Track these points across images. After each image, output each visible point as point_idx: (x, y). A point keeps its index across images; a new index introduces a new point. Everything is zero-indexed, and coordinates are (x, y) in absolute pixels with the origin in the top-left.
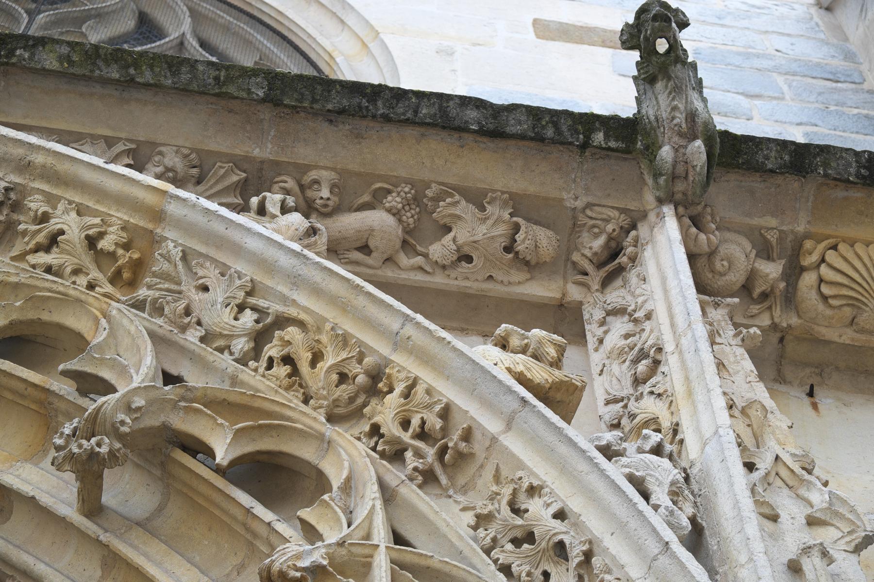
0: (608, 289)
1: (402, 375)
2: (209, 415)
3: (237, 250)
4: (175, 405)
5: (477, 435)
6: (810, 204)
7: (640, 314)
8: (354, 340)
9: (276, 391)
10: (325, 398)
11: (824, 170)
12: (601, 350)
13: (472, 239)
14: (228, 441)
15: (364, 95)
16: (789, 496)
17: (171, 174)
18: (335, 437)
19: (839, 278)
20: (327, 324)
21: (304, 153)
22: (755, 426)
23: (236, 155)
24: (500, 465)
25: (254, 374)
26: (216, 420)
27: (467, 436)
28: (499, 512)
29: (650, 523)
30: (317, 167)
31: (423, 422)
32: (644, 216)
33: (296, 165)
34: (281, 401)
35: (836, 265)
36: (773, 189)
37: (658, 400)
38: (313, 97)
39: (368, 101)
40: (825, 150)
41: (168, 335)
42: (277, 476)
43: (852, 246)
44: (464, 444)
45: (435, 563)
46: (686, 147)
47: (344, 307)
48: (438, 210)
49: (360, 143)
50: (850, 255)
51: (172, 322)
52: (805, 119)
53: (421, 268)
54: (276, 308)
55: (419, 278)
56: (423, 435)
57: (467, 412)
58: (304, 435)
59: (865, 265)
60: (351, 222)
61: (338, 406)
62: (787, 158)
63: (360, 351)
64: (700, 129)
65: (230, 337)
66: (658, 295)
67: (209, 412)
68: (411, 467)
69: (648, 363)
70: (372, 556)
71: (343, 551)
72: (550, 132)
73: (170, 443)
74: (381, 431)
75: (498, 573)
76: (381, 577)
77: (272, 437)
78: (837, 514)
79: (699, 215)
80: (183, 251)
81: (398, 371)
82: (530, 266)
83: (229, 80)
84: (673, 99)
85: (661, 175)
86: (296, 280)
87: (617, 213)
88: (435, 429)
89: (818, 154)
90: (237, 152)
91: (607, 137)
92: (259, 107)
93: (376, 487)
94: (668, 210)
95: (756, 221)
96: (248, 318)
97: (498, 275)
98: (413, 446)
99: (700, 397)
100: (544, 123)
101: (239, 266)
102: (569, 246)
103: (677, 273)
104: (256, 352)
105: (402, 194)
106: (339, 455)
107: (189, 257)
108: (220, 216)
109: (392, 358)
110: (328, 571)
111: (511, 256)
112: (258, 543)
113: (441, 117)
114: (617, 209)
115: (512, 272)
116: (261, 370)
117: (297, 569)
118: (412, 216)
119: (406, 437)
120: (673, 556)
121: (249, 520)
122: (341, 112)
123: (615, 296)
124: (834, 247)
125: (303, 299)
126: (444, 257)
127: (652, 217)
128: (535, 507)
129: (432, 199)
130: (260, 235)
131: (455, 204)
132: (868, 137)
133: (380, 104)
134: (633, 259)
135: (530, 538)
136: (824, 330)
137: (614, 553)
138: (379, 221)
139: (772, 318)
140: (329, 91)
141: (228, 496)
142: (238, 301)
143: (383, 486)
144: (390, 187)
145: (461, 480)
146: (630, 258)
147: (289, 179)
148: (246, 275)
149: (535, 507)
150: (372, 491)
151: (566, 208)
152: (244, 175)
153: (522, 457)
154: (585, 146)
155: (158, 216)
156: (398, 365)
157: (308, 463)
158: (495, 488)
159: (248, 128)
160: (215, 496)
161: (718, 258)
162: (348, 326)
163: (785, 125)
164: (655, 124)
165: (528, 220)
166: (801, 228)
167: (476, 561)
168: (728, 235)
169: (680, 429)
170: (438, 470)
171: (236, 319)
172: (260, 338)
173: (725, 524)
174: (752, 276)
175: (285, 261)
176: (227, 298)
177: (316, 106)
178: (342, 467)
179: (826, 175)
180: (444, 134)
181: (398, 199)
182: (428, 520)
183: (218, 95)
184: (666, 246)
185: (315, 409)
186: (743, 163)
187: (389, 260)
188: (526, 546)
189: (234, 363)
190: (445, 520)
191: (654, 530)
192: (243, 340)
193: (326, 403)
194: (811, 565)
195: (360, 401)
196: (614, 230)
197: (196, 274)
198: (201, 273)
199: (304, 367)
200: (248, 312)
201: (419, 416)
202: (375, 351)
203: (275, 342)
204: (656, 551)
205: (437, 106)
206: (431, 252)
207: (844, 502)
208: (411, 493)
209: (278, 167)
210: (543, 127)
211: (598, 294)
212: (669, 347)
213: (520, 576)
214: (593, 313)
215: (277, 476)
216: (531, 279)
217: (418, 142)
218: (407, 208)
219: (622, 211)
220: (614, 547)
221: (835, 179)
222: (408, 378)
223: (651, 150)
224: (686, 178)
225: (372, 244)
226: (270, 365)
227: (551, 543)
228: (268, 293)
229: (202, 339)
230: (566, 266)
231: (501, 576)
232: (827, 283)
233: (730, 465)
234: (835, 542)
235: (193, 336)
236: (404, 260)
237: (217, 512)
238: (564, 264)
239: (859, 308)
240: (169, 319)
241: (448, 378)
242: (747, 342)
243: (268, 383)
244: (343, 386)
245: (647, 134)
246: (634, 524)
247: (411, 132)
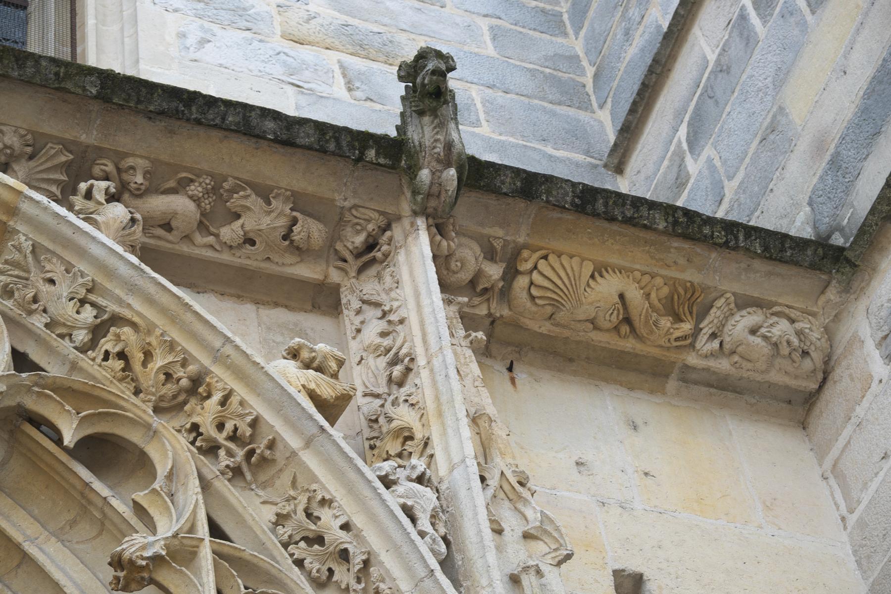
0: (363, 277)
1: (220, 385)
2: (58, 402)
3: (82, 253)
4: (29, 389)
5: (280, 446)
6: (531, 220)
7: (393, 317)
8: (180, 348)
9: (111, 382)
10: (153, 394)
11: (547, 197)
12: (358, 339)
13: (257, 227)
14: (74, 426)
15: (181, 100)
16: (510, 509)
17: (8, 151)
18: (161, 429)
19: (546, 283)
20: (157, 329)
21: (123, 142)
22: (483, 435)
23: (66, 139)
25: (92, 363)
26: (64, 406)
27: (271, 445)
28: (295, 513)
29: (419, 551)
30: (133, 155)
31: (236, 429)
32: (399, 218)
33: (116, 152)
34: (113, 391)
35: (545, 273)
37: (411, 409)
38: (138, 99)
39: (184, 106)
40: (549, 179)
41: (17, 317)
42: (106, 452)
43: (559, 257)
44: (269, 452)
45: (246, 556)
46: (441, 172)
47: (173, 319)
48: (232, 200)
49: (172, 138)
50: (557, 266)
51: (19, 305)
52: (490, 12)
53: (212, 246)
54: (113, 307)
55: (210, 254)
56: (233, 437)
57: (273, 427)
58: (132, 422)
59: (567, 274)
60: (159, 204)
61: (163, 401)
62: (519, 184)
63: (184, 358)
64: (455, 158)
65: (73, 328)
66: (411, 304)
67: (58, 399)
68: (224, 464)
69: (401, 369)
70: (198, 547)
71: (176, 542)
72: (332, 146)
73: (20, 416)
74: (201, 430)
75: (294, 566)
76: (208, 570)
78: (546, 532)
79: (443, 223)
80: (33, 245)
81: (217, 382)
82: (300, 251)
83: (68, 76)
84: (437, 133)
85: (419, 193)
86: (133, 289)
87: (376, 215)
88: (244, 435)
89: (543, 183)
90: (67, 136)
91: (378, 154)
92: (90, 101)
93: (197, 482)
94: (421, 222)
95: (487, 231)
96: (88, 314)
97: (276, 258)
98: (226, 447)
99: (449, 422)
100: (328, 138)
101: (82, 266)
102: (333, 238)
103: (429, 292)
104: (93, 344)
105: (203, 184)
106: (163, 444)
107: (37, 250)
108: (68, 221)
109: (213, 369)
110: (165, 559)
111: (287, 243)
112: (92, 509)
113: (244, 125)
114: (378, 211)
115: (286, 255)
116: (99, 360)
117: (143, 558)
118: (210, 203)
119: (221, 438)
120: (437, 581)
121: (87, 491)
122: (161, 113)
123: (369, 287)
124: (545, 257)
125: (137, 304)
126: (232, 239)
127: (406, 222)
128: (325, 514)
129: (228, 191)
130: (104, 245)
131: (246, 197)
132: (544, 35)
133: (194, 109)
134: (386, 256)
135: (319, 540)
136: (527, 322)
137: (388, 567)
138: (181, 205)
139: (489, 309)
140: (152, 94)
141: (71, 469)
142: (80, 297)
143: (201, 477)
144: (190, 176)
145: (262, 477)
146: (384, 255)
147: (109, 164)
148: (88, 275)
149: (325, 514)
150: (194, 484)
151: (336, 206)
152: (71, 157)
153: (317, 473)
154: (360, 159)
155: (13, 211)
156: (217, 376)
157: (136, 446)
158: (292, 493)
159: (78, 116)
160: (60, 469)
161: (454, 259)
162: (175, 334)
163: (474, 16)
164: (418, 148)
165: (303, 212)
166: (521, 240)
167: (276, 553)
168: (464, 240)
169: (430, 443)
170: (245, 468)
171: (78, 312)
172: (98, 331)
173: (470, 546)
174: (479, 275)
175: (123, 270)
176: (71, 293)
177: (139, 106)
178: (165, 455)
179: (548, 202)
180: (244, 138)
181: (200, 189)
182: (237, 512)
183: (57, 89)
184: (415, 257)
185: (144, 402)
186: (484, 186)
187: (187, 238)
188: (316, 547)
189: (75, 351)
190: (251, 515)
191: (423, 557)
192: (84, 332)
193: (154, 398)
194: (528, 580)
195: (181, 398)
196: (374, 230)
197: (44, 267)
198: (48, 267)
199: (137, 366)
200: (87, 306)
201: (233, 422)
202: (198, 360)
203: (110, 336)
204: (423, 575)
205: (241, 115)
206: (222, 234)
207: (552, 521)
208: (222, 485)
209: (100, 152)
210: (327, 141)
211: (354, 280)
212: (421, 361)
213: (311, 572)
214: (350, 300)
215: (106, 452)
216: (302, 261)
217: (221, 141)
218: (206, 196)
219: (381, 213)
220: (387, 560)
221: (554, 205)
222: (225, 389)
223: (412, 171)
224: (439, 196)
225: (174, 224)
226: (107, 356)
227: (338, 549)
228: (105, 293)
229: (47, 325)
230: (329, 252)
231: (296, 569)
232: (536, 286)
233: (475, 495)
234: (544, 556)
235: (38, 322)
236: (199, 239)
237: (57, 478)
238: (330, 251)
239: (558, 307)
240: (18, 302)
241: (259, 395)
242: (474, 344)
243: (104, 373)
244: (169, 386)
245: (410, 156)
246: (406, 548)
247: (215, 134)
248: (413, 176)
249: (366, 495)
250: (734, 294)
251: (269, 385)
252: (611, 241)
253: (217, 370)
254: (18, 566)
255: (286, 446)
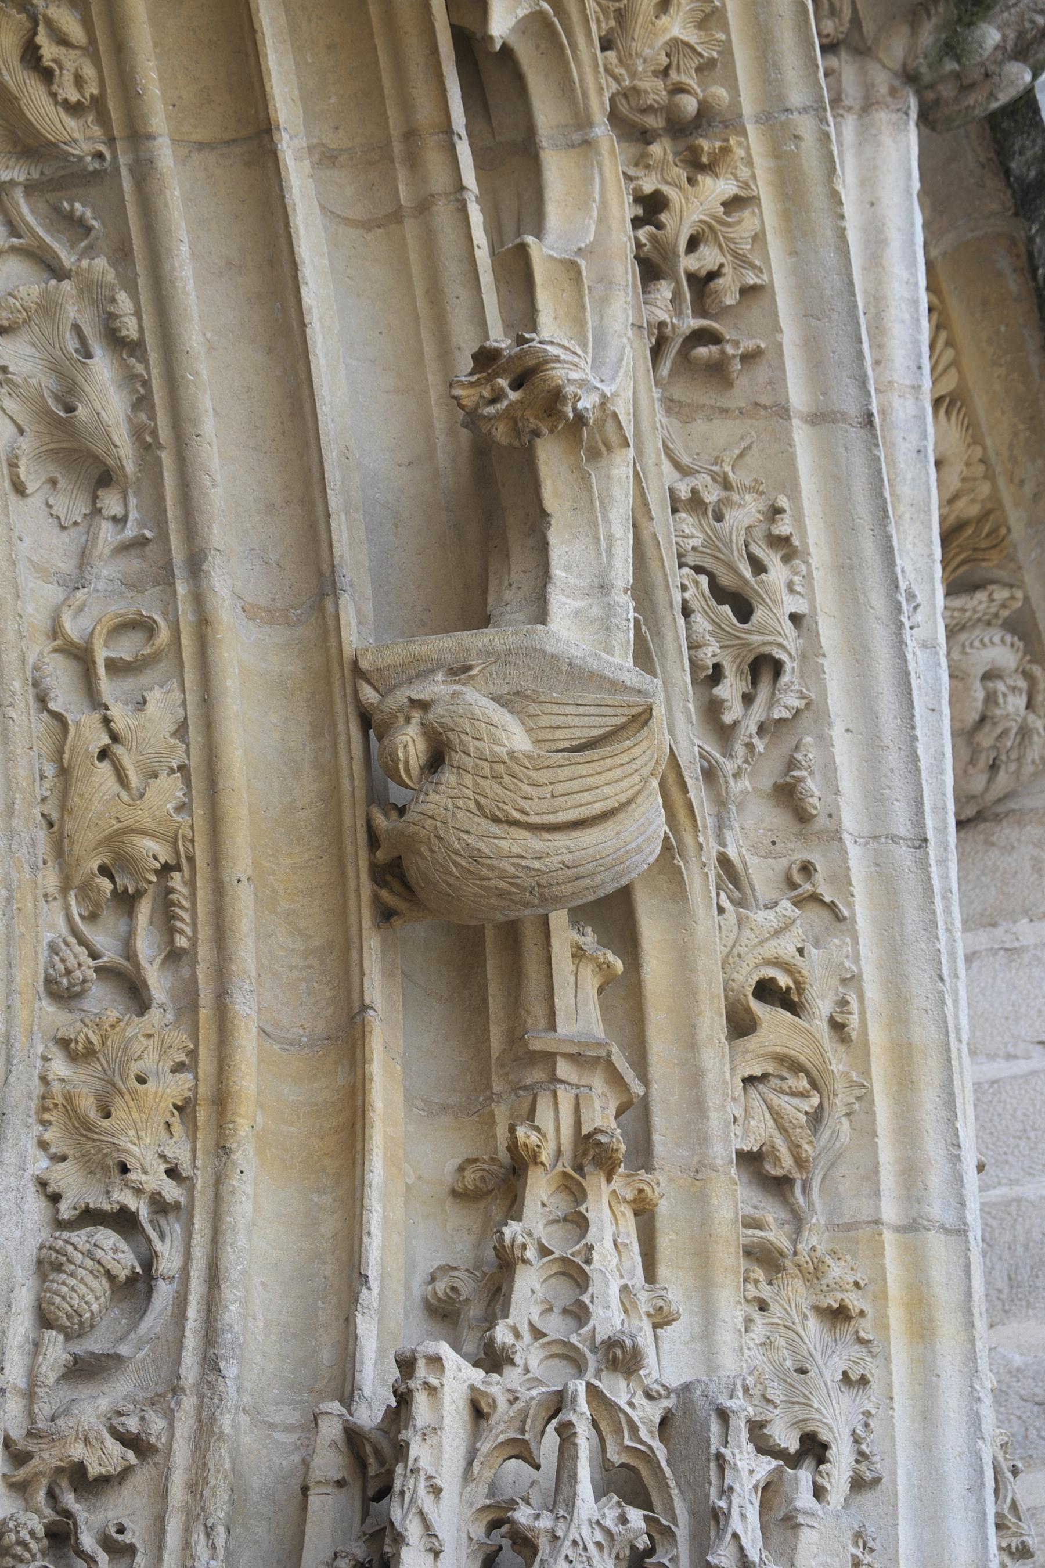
1: (744, 173)
5: (762, 372)
6: (969, 236)
10: (633, 75)
24: (755, 447)
36: (972, 181)
58: (567, 88)
62: (1033, 174)
74: (663, 217)
77: (537, 47)
106: (589, 180)
109: (750, 128)
135: (744, 610)
170: (672, 351)
195: (655, 122)
222: (746, 185)
227: (766, 650)
248: (966, 20)
249: (874, 603)
250: (1026, 599)
251: (829, 256)
252: (1003, 371)
253: (755, 141)
254: (201, 146)
255: (778, 381)
